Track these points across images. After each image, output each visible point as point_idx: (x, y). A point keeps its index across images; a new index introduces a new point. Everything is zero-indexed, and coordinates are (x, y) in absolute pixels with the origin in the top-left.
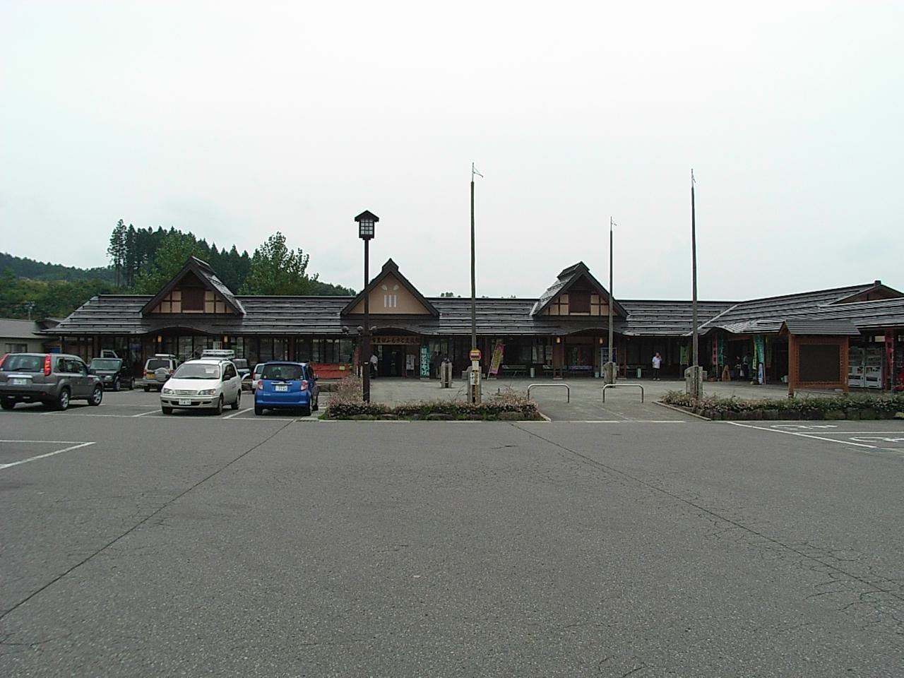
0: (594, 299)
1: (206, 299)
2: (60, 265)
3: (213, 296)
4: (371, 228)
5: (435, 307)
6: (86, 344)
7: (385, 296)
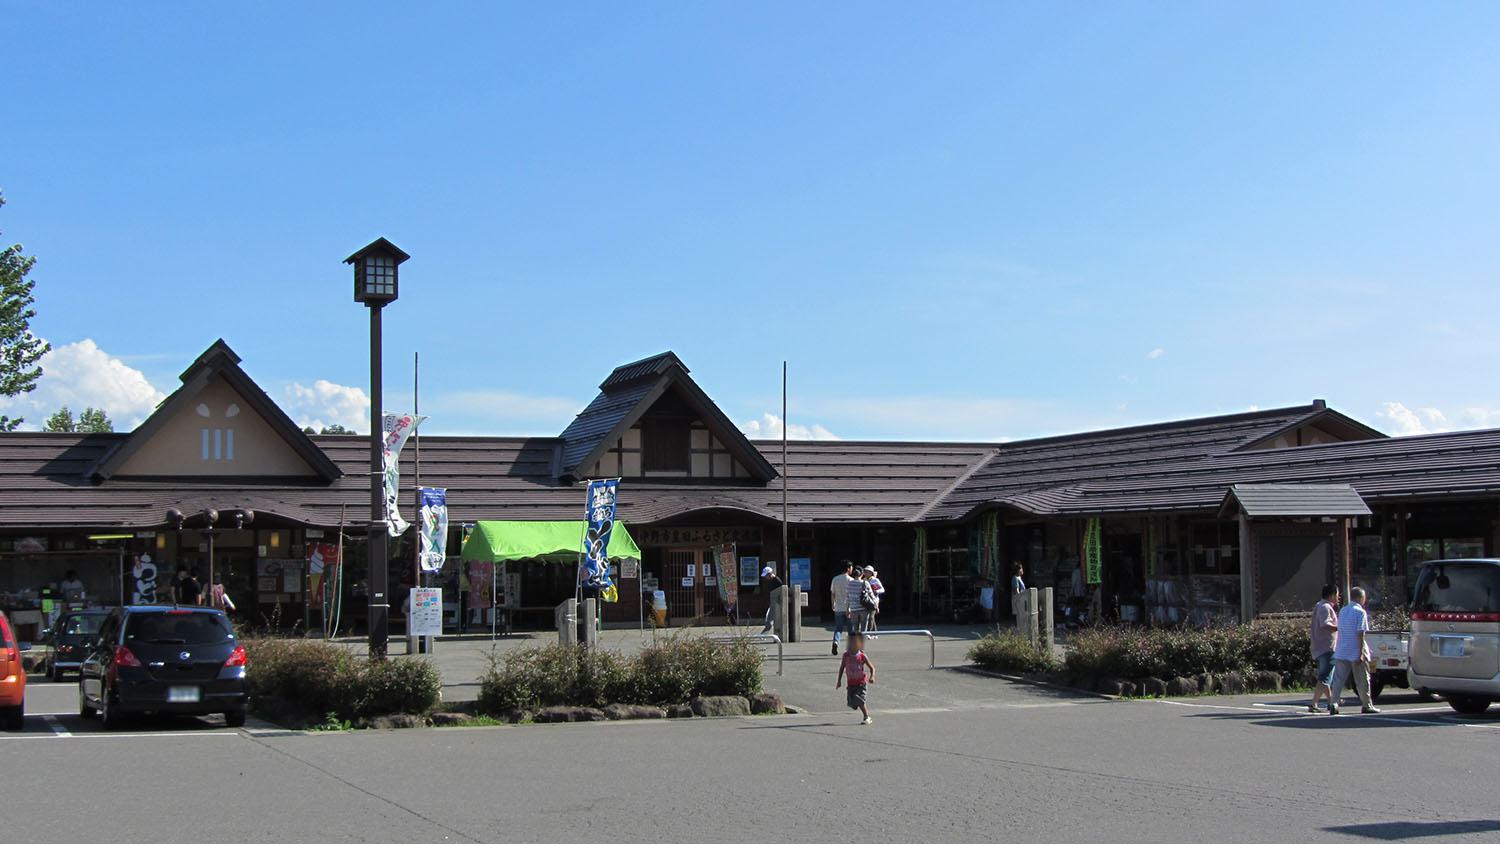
0: (698, 440)
1: (693, 446)
2: (617, 372)
3: (707, 441)
4: (390, 280)
5: (770, 461)
6: (1415, 557)
7: (206, 433)
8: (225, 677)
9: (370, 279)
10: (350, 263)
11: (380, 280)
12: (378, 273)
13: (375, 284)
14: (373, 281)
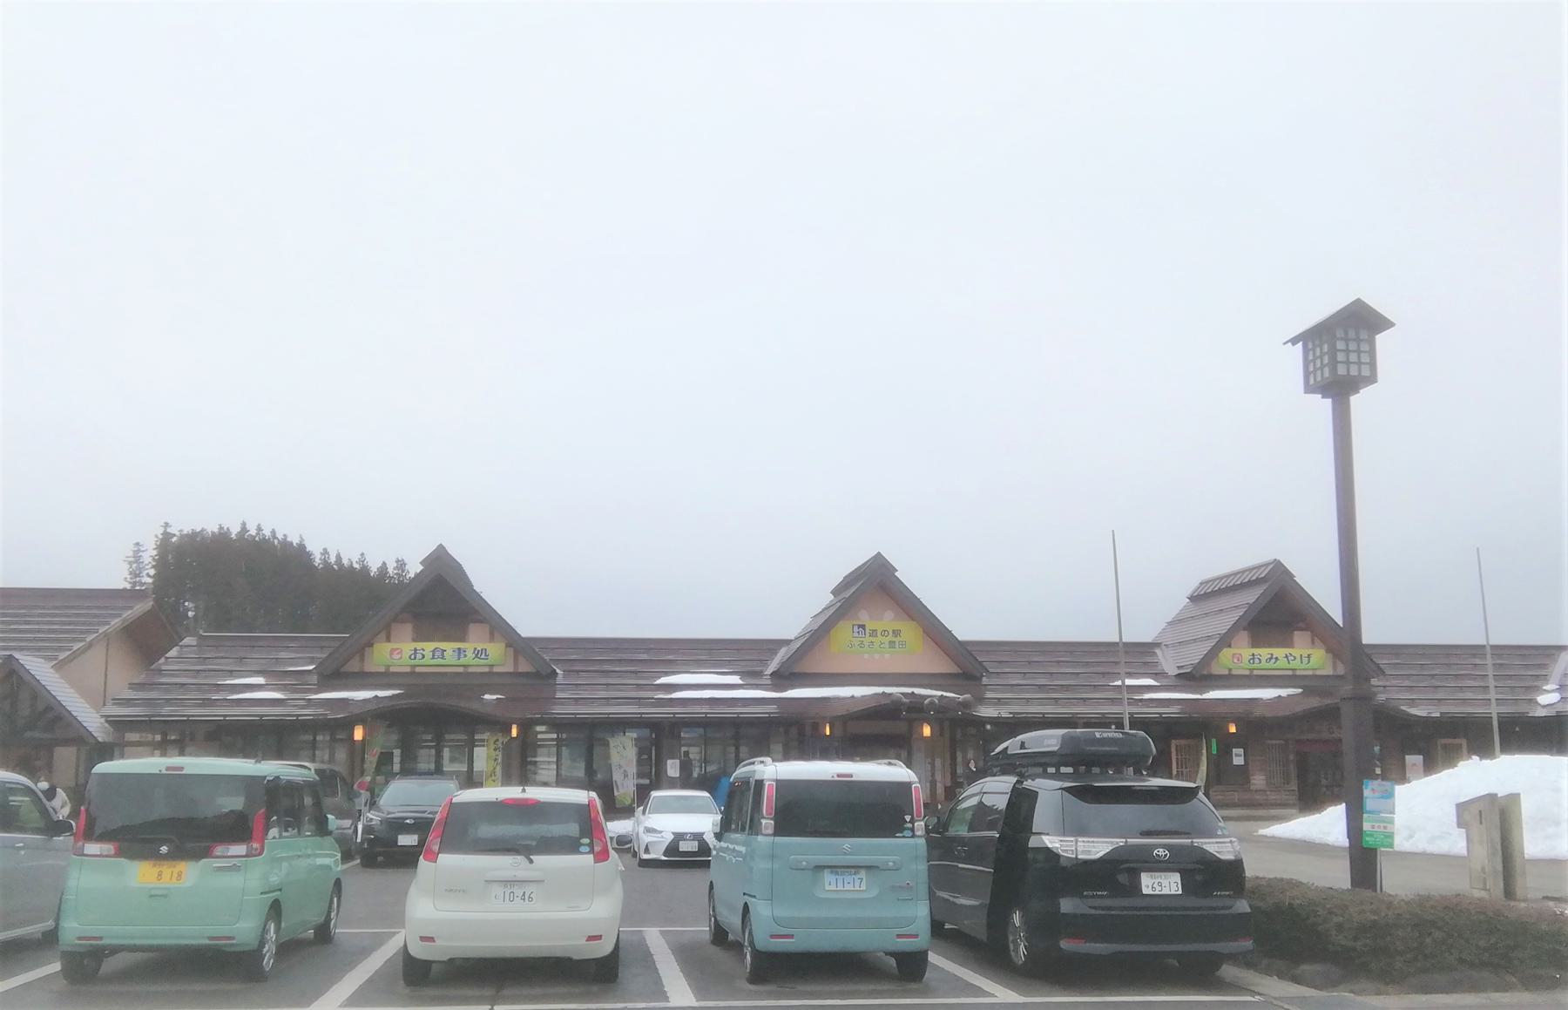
8: (1466, 849)
9: (1341, 357)
10: (1293, 345)
11: (1353, 357)
12: (1351, 348)
13: (1348, 363)
14: (1344, 359)
